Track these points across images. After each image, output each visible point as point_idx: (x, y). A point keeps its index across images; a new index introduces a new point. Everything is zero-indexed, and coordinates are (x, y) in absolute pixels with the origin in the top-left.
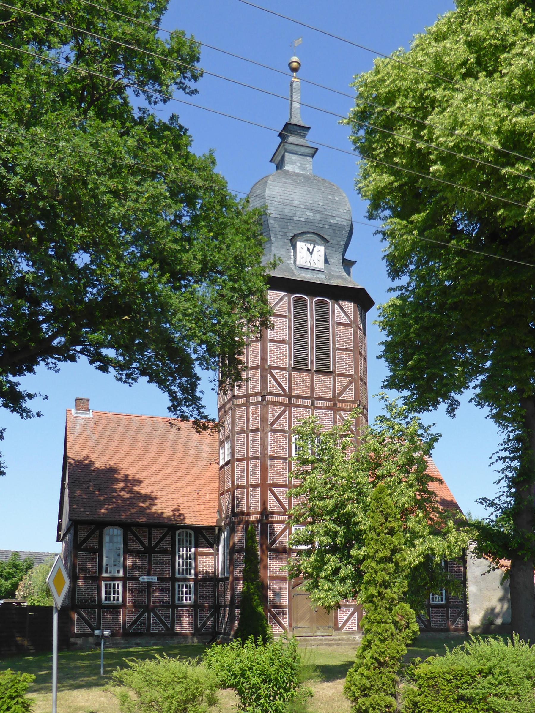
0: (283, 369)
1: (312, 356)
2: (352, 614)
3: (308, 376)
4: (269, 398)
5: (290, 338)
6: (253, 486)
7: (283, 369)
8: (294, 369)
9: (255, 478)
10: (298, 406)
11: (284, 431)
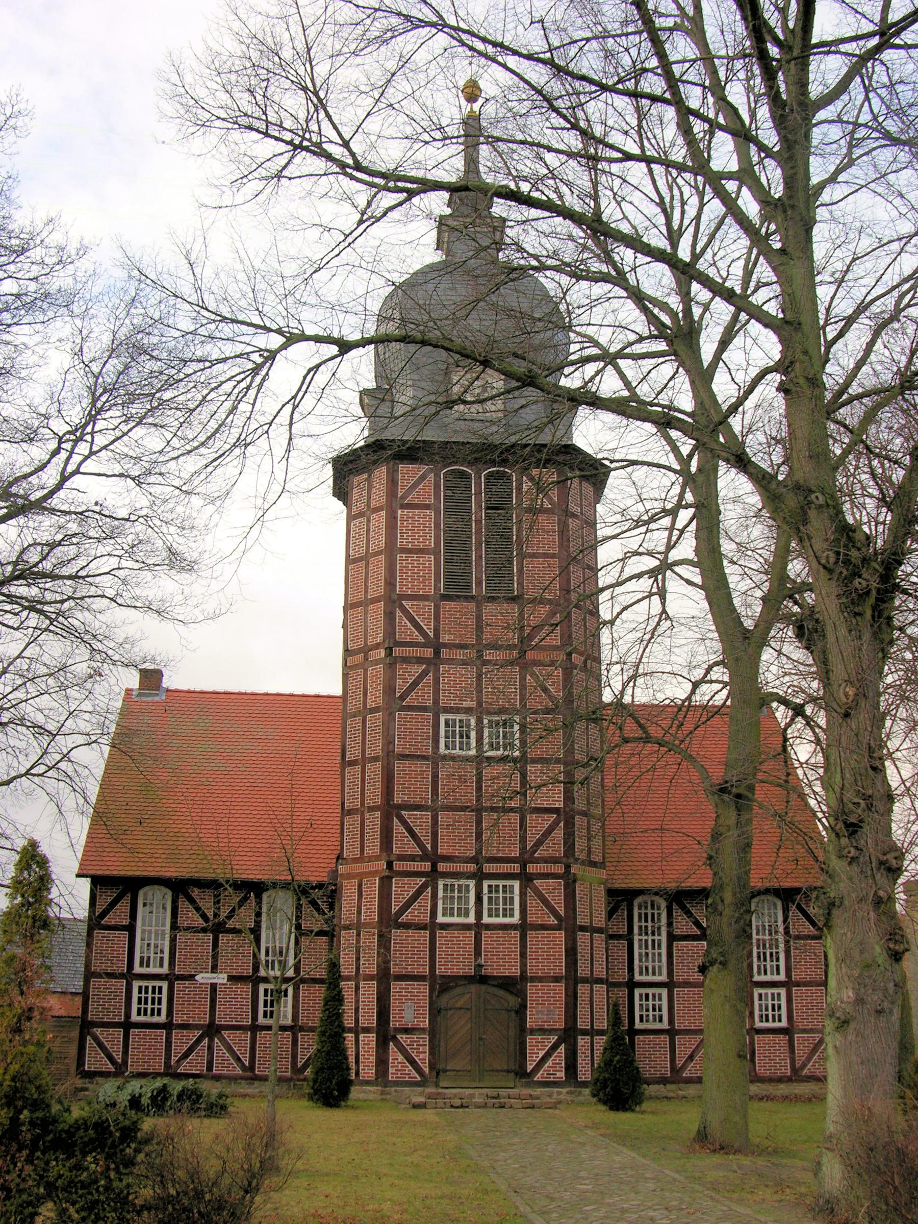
0: (425, 598)
1: (478, 572)
2: (555, 1047)
3: (472, 606)
4: (397, 651)
5: (437, 543)
6: (372, 809)
7: (425, 598)
8: (445, 597)
9: (374, 796)
10: (450, 661)
11: (424, 709)
